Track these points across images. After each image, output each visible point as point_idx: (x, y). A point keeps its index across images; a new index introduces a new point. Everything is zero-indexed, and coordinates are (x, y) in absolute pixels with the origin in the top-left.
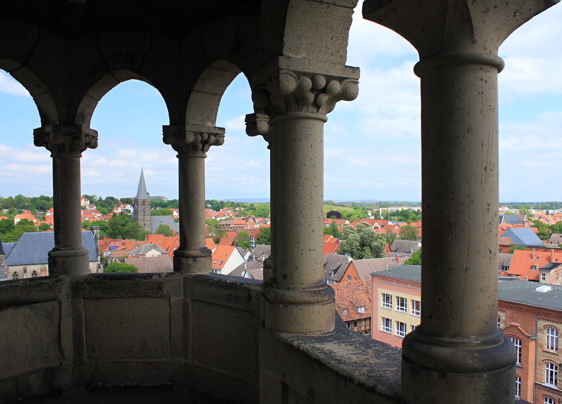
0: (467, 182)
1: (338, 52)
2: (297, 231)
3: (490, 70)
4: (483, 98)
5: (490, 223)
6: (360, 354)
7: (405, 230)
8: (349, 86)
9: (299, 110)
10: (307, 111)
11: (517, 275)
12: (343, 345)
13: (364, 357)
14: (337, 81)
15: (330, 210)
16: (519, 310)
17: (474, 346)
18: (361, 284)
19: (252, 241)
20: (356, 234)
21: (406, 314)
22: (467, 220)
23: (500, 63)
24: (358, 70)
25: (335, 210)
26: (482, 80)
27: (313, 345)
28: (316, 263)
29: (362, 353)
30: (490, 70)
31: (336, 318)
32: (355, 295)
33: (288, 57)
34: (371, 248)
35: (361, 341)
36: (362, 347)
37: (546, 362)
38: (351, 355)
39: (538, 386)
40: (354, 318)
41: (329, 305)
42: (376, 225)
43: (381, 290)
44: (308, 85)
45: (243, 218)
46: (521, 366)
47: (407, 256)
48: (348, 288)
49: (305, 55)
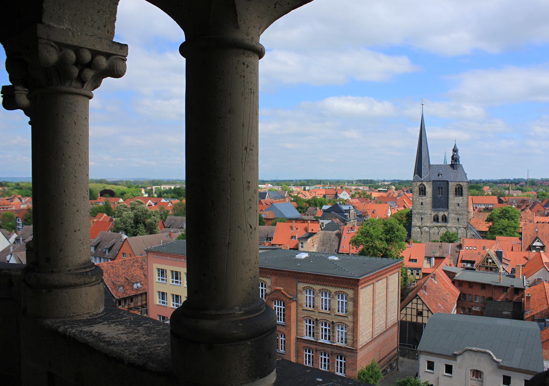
0: (228, 161)
1: (105, 27)
2: (60, 212)
3: (252, 55)
4: (245, 81)
5: (250, 200)
6: (130, 333)
7: (178, 206)
8: (116, 63)
9: (61, 84)
10: (71, 85)
11: (279, 245)
12: (113, 325)
13: (135, 335)
14: (103, 57)
15: (103, 189)
16: (282, 276)
17: (238, 317)
18: (136, 261)
19: (18, 222)
20: (130, 212)
21: (180, 286)
22: (229, 197)
23: (261, 50)
24: (126, 47)
25: (108, 189)
26: (244, 64)
27: (80, 329)
28: (82, 243)
29: (132, 332)
30: (252, 55)
31: (105, 298)
32: (130, 272)
33: (49, 26)
34: (145, 225)
35: (132, 319)
36: (133, 326)
37: (305, 319)
38: (121, 335)
39: (299, 340)
40: (130, 294)
41: (97, 286)
42: (150, 203)
43: (155, 266)
44: (72, 58)
45: (7, 198)
46: (285, 325)
47: (180, 232)
48: (123, 265)
49: (68, 26)
